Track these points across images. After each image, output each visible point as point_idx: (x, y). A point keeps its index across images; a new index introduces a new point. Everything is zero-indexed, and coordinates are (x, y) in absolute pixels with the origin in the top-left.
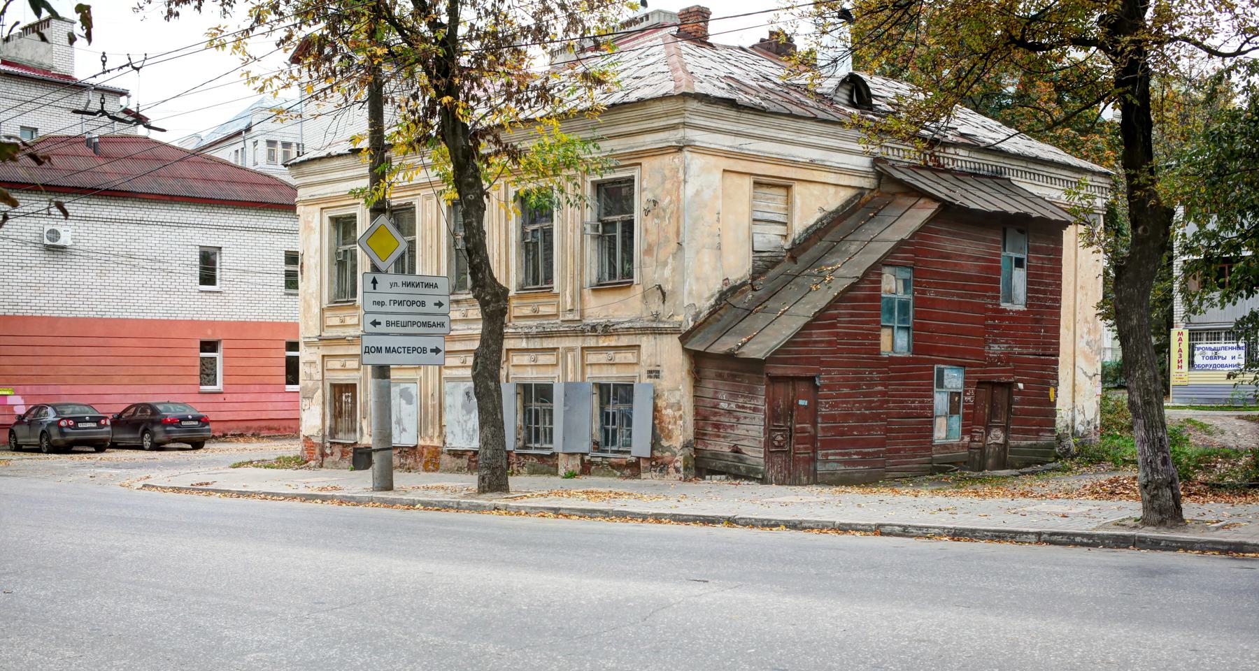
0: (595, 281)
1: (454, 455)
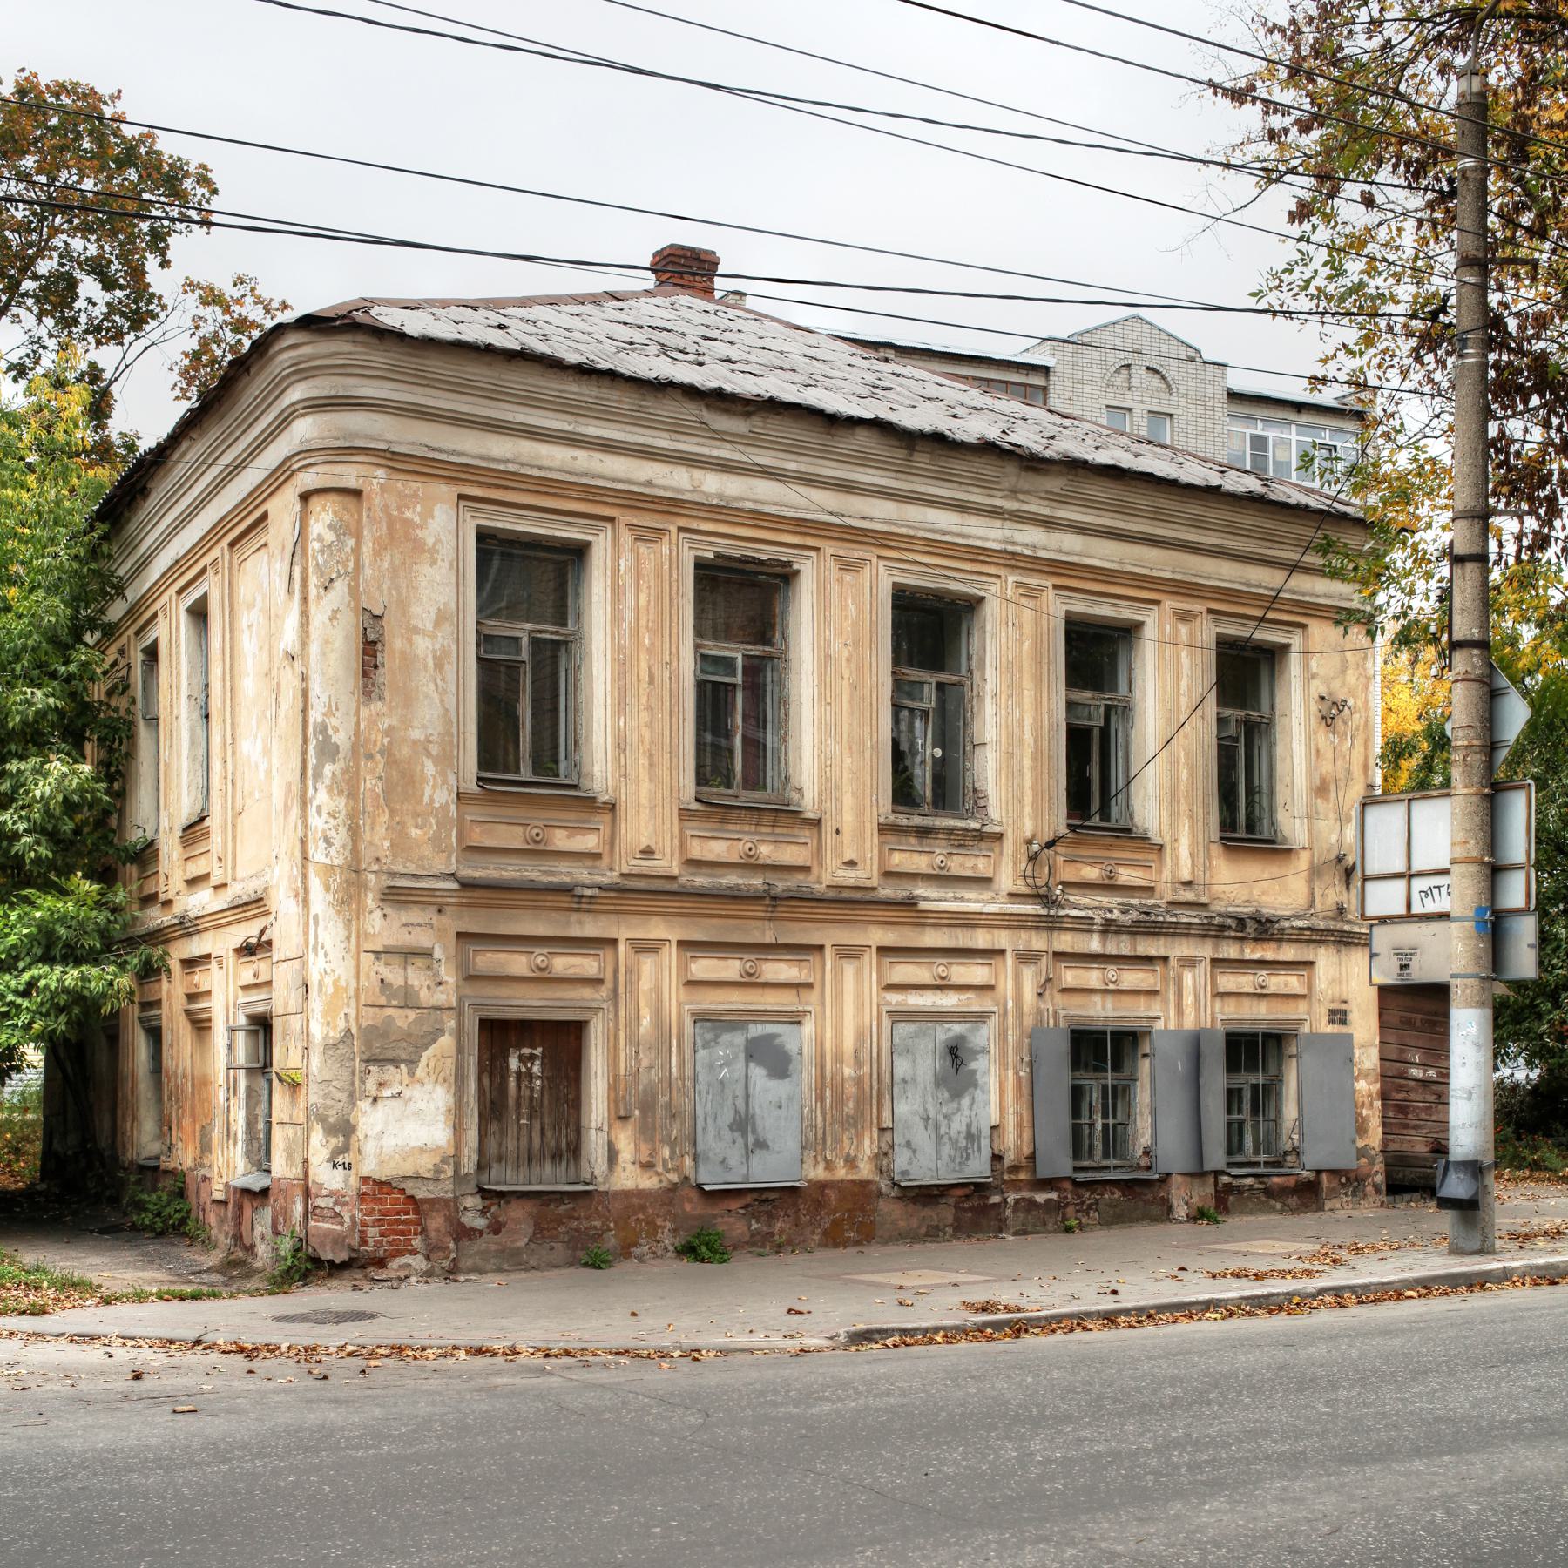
1: (914, 1200)
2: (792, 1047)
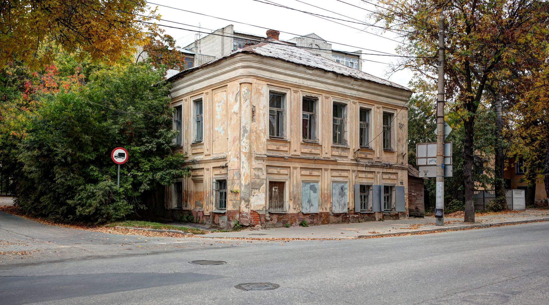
2: (317, 187)
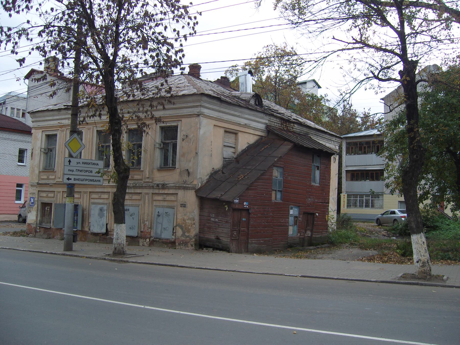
0: (159, 166)
